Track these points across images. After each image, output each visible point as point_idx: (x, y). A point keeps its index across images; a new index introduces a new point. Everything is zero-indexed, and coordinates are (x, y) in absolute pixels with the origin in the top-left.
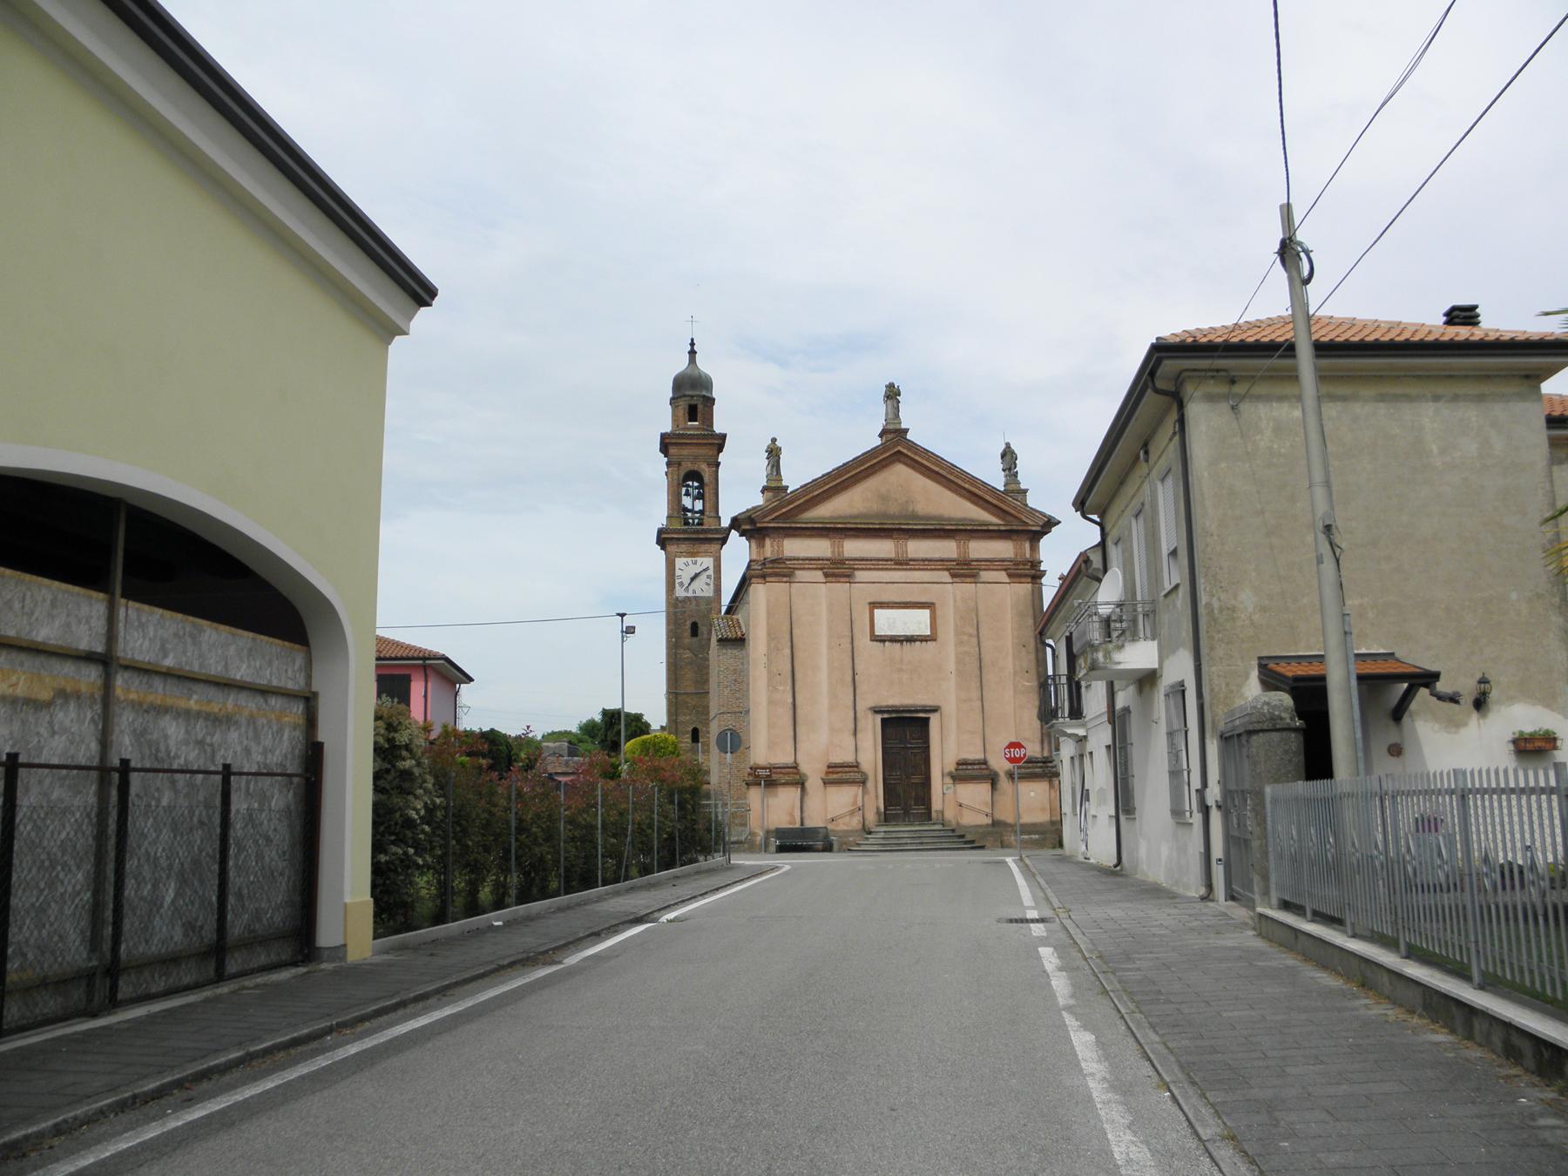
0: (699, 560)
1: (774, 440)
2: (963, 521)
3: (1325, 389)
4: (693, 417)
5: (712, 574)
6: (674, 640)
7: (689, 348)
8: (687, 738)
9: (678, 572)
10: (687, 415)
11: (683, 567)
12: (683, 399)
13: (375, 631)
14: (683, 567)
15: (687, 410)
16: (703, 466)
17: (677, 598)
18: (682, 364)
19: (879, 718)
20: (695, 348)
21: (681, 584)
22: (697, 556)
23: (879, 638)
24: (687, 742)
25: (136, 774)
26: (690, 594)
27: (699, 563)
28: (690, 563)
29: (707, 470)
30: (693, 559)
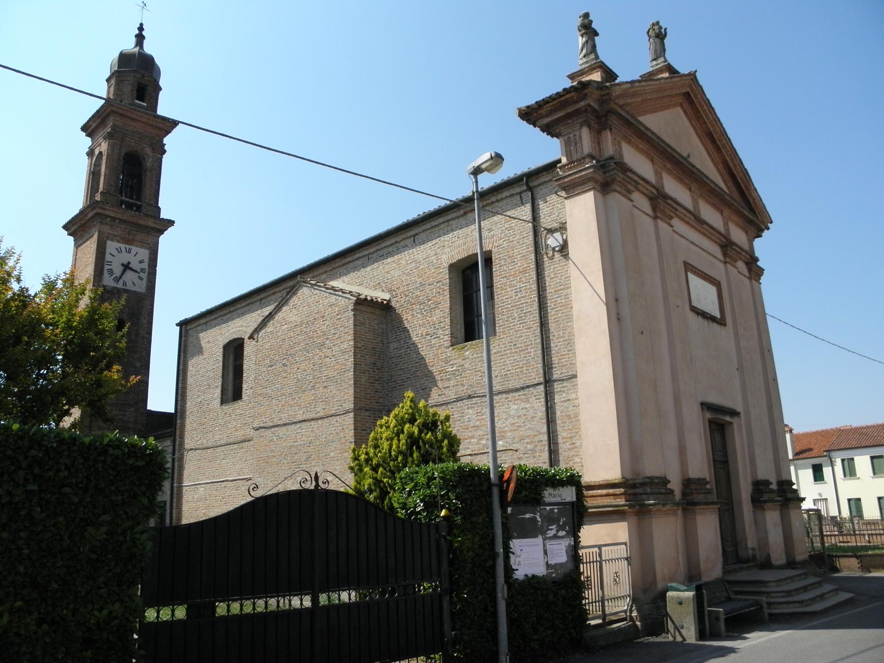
0: (134, 249)
1: (586, 15)
2: (720, 186)
3: (477, 337)
4: (141, 97)
5: (147, 267)
7: (137, 32)
9: (108, 258)
10: (135, 91)
11: (115, 252)
13: (180, 621)
14: (115, 252)
15: (136, 88)
16: (147, 149)
19: (858, 477)
20: (144, 33)
21: (111, 272)
22: (132, 244)
23: (696, 310)
25: (607, 608)
26: (120, 285)
27: (133, 252)
28: (123, 250)
29: (151, 155)
30: (128, 247)
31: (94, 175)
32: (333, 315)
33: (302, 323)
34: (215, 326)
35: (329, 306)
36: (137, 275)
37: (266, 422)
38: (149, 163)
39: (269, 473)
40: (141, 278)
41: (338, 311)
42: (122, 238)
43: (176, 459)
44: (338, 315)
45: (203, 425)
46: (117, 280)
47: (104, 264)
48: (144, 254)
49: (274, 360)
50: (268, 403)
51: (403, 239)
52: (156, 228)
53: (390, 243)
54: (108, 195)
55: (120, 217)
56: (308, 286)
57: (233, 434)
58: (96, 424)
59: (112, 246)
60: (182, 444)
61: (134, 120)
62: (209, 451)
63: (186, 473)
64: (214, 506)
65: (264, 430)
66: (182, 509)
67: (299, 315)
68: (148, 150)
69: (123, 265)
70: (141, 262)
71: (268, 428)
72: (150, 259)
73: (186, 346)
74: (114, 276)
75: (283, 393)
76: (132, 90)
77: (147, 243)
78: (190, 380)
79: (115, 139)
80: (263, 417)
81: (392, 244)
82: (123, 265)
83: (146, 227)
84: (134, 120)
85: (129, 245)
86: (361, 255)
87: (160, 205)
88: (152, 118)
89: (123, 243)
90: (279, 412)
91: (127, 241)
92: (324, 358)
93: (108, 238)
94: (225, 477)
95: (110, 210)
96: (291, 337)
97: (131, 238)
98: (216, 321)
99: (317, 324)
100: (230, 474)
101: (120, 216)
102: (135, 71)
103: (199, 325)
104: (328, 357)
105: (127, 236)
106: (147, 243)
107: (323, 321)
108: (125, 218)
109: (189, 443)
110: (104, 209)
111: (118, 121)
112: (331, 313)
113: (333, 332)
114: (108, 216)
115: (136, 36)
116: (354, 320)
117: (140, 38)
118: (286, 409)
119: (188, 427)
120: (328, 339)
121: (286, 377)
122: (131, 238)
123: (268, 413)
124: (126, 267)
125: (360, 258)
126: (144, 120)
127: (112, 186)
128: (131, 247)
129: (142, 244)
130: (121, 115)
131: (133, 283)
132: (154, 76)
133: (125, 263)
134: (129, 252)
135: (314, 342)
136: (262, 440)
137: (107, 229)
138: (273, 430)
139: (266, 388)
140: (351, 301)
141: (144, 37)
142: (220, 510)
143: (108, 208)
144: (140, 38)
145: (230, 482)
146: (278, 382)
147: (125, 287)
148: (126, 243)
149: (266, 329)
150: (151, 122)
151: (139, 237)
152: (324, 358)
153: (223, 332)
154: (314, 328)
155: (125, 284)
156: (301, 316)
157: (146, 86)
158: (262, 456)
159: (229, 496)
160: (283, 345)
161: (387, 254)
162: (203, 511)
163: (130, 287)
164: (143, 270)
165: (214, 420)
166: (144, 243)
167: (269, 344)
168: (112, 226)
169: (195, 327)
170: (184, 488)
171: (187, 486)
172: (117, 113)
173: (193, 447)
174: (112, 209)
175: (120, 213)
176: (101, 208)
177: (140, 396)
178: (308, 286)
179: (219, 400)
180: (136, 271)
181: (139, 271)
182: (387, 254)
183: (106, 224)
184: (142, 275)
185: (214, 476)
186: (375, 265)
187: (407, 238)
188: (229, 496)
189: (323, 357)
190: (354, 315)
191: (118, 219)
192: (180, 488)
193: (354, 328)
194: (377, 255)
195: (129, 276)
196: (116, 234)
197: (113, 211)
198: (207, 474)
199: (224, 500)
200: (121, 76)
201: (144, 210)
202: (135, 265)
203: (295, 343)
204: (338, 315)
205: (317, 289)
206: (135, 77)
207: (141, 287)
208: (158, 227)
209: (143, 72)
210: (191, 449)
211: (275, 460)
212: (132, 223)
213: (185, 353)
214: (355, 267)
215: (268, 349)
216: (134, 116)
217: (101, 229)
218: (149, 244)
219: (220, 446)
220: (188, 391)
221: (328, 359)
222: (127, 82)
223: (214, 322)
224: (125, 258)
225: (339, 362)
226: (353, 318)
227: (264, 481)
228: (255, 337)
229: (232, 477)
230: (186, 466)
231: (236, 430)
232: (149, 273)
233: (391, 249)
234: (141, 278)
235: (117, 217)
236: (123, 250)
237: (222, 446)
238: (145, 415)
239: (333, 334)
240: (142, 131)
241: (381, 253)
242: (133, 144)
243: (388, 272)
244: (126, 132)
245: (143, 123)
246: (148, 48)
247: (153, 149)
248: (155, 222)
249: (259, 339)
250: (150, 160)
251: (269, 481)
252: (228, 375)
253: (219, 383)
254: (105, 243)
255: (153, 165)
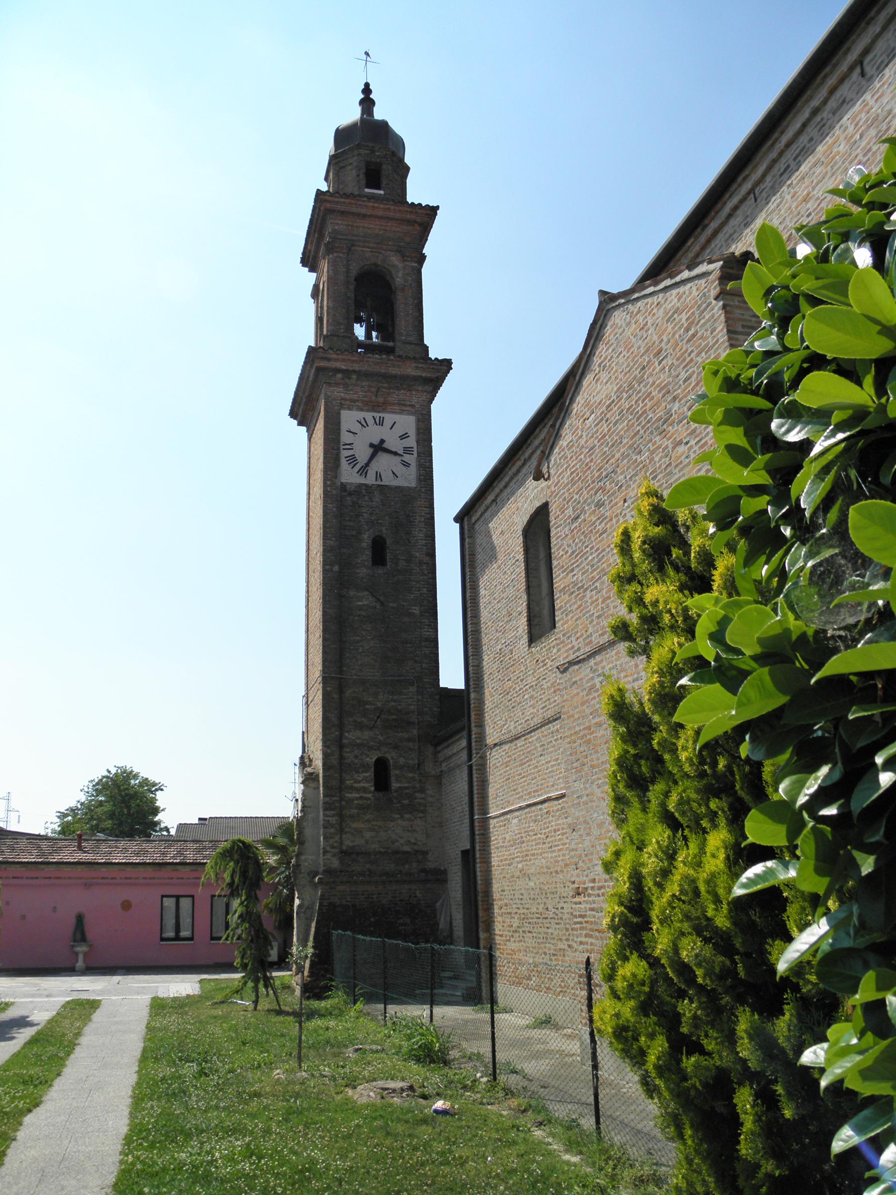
0: (389, 418)
6: (336, 568)
8: (365, 779)
9: (345, 437)
10: (362, 176)
11: (356, 428)
12: (356, 152)
14: (356, 428)
15: (363, 171)
17: (343, 487)
18: (354, 114)
21: (352, 460)
22: (384, 410)
24: (365, 790)
26: (370, 480)
28: (370, 421)
29: (401, 265)
30: (377, 415)
31: (319, 320)
32: (677, 336)
33: (620, 390)
34: (509, 499)
35: (668, 321)
36: (398, 459)
37: (579, 649)
38: (399, 279)
39: (593, 767)
40: (406, 464)
41: (687, 320)
42: (366, 403)
43: (474, 768)
44: (687, 330)
45: (508, 694)
46: (363, 471)
47: (339, 449)
48: (407, 423)
49: (579, 502)
50: (579, 603)
51: (832, 91)
52: (420, 377)
53: (797, 125)
54: (335, 338)
55: (357, 369)
56: (620, 305)
57: (552, 700)
58: (351, 720)
59: (349, 418)
60: (482, 737)
61: (364, 216)
62: (519, 743)
63: (491, 791)
64: (534, 855)
65: (576, 667)
66: (490, 863)
67: (613, 378)
68: (395, 260)
69: (371, 445)
70: (403, 437)
71: (584, 660)
72: (418, 433)
73: (473, 555)
74: (358, 467)
75: (603, 570)
76: (358, 175)
77: (410, 405)
78: (484, 614)
79: (337, 252)
80: (573, 639)
81: (804, 125)
82: (371, 445)
83: (404, 378)
84: (364, 216)
85: (379, 412)
86: (735, 200)
87: (426, 342)
88: (392, 208)
89: (368, 411)
90: (598, 617)
91: (374, 407)
92: (674, 448)
93: (342, 406)
94: (546, 793)
95: (336, 360)
96: (605, 436)
97: (381, 400)
98: (508, 490)
99: (651, 375)
100: (553, 786)
101: (356, 367)
102: (358, 146)
103: (487, 508)
104: (680, 443)
105: (373, 398)
106: (410, 405)
107: (660, 363)
108: (365, 368)
109: (492, 735)
110: (329, 360)
111: (338, 224)
112: (674, 334)
113: (683, 375)
114: (338, 371)
115: (362, 102)
116: (727, 320)
117: (367, 103)
118: (611, 605)
119: (488, 704)
120: (674, 399)
121: (605, 531)
122: (381, 400)
123: (580, 627)
124: (378, 448)
125: (736, 208)
126: (380, 213)
127: (341, 324)
128: (382, 415)
129: (403, 407)
130: (343, 213)
131: (393, 473)
132: (392, 147)
133: (376, 442)
134: (381, 423)
135: (648, 422)
136: (575, 692)
137: (338, 392)
138: (592, 662)
139: (572, 570)
140: (711, 277)
141: (373, 103)
142: (544, 861)
143: (334, 356)
144: (367, 103)
145: (556, 802)
146: (592, 548)
147: (379, 483)
148: (373, 410)
149: (561, 442)
150: (391, 214)
151: (394, 397)
152: (674, 448)
153: (520, 504)
154: (643, 390)
155: (378, 476)
156: (616, 378)
157: (381, 164)
158: (577, 729)
159: (555, 831)
160: (591, 461)
161: (795, 159)
162: (520, 866)
163: (388, 480)
164: (408, 450)
165: (522, 680)
166: (405, 405)
167: (569, 473)
168: (346, 386)
169: (481, 516)
170: (491, 821)
171: (495, 818)
172: (334, 211)
173: (497, 741)
174: (340, 357)
175: (356, 361)
176: (323, 358)
177: (424, 665)
178: (620, 305)
179: (525, 639)
180: (395, 454)
181: (401, 452)
182: (795, 159)
183: (337, 384)
184: (407, 458)
185: (530, 793)
186: (775, 200)
187: (842, 81)
188: (555, 831)
189: (670, 446)
190: (724, 307)
191: (354, 371)
192: (485, 821)
193: (730, 339)
194: (774, 176)
195: (383, 463)
196: (355, 397)
197: (344, 360)
198: (520, 790)
199: (548, 840)
200: (339, 162)
201: (398, 352)
202: (393, 443)
203: (613, 445)
204: (687, 330)
205: (638, 299)
206: (359, 155)
207: (408, 478)
208: (424, 375)
209: (370, 144)
210: (495, 745)
211: (602, 732)
212: (379, 375)
213: (473, 566)
214: (731, 235)
215: (568, 484)
216: (363, 211)
217: (329, 394)
218: (412, 406)
219: (534, 730)
220: (483, 635)
221: (682, 449)
222: (350, 167)
223: (505, 494)
224: (374, 434)
225: (706, 443)
226: (723, 318)
227: (586, 788)
228: (545, 470)
229: (557, 790)
230: (491, 779)
231: (555, 692)
232: (418, 453)
233: (803, 139)
234: (406, 464)
235: (351, 369)
236: (370, 421)
237: (537, 729)
238: (437, 697)
239: (685, 381)
240: (381, 232)
241: (781, 166)
242: (368, 255)
243: (806, 200)
244: (354, 238)
245: (381, 218)
246: (379, 114)
247: (403, 256)
248: (417, 368)
249: (552, 471)
250: (400, 275)
251: (594, 786)
252: (540, 586)
253: (522, 605)
254: (339, 414)
255: (406, 281)
